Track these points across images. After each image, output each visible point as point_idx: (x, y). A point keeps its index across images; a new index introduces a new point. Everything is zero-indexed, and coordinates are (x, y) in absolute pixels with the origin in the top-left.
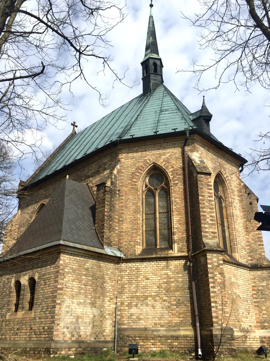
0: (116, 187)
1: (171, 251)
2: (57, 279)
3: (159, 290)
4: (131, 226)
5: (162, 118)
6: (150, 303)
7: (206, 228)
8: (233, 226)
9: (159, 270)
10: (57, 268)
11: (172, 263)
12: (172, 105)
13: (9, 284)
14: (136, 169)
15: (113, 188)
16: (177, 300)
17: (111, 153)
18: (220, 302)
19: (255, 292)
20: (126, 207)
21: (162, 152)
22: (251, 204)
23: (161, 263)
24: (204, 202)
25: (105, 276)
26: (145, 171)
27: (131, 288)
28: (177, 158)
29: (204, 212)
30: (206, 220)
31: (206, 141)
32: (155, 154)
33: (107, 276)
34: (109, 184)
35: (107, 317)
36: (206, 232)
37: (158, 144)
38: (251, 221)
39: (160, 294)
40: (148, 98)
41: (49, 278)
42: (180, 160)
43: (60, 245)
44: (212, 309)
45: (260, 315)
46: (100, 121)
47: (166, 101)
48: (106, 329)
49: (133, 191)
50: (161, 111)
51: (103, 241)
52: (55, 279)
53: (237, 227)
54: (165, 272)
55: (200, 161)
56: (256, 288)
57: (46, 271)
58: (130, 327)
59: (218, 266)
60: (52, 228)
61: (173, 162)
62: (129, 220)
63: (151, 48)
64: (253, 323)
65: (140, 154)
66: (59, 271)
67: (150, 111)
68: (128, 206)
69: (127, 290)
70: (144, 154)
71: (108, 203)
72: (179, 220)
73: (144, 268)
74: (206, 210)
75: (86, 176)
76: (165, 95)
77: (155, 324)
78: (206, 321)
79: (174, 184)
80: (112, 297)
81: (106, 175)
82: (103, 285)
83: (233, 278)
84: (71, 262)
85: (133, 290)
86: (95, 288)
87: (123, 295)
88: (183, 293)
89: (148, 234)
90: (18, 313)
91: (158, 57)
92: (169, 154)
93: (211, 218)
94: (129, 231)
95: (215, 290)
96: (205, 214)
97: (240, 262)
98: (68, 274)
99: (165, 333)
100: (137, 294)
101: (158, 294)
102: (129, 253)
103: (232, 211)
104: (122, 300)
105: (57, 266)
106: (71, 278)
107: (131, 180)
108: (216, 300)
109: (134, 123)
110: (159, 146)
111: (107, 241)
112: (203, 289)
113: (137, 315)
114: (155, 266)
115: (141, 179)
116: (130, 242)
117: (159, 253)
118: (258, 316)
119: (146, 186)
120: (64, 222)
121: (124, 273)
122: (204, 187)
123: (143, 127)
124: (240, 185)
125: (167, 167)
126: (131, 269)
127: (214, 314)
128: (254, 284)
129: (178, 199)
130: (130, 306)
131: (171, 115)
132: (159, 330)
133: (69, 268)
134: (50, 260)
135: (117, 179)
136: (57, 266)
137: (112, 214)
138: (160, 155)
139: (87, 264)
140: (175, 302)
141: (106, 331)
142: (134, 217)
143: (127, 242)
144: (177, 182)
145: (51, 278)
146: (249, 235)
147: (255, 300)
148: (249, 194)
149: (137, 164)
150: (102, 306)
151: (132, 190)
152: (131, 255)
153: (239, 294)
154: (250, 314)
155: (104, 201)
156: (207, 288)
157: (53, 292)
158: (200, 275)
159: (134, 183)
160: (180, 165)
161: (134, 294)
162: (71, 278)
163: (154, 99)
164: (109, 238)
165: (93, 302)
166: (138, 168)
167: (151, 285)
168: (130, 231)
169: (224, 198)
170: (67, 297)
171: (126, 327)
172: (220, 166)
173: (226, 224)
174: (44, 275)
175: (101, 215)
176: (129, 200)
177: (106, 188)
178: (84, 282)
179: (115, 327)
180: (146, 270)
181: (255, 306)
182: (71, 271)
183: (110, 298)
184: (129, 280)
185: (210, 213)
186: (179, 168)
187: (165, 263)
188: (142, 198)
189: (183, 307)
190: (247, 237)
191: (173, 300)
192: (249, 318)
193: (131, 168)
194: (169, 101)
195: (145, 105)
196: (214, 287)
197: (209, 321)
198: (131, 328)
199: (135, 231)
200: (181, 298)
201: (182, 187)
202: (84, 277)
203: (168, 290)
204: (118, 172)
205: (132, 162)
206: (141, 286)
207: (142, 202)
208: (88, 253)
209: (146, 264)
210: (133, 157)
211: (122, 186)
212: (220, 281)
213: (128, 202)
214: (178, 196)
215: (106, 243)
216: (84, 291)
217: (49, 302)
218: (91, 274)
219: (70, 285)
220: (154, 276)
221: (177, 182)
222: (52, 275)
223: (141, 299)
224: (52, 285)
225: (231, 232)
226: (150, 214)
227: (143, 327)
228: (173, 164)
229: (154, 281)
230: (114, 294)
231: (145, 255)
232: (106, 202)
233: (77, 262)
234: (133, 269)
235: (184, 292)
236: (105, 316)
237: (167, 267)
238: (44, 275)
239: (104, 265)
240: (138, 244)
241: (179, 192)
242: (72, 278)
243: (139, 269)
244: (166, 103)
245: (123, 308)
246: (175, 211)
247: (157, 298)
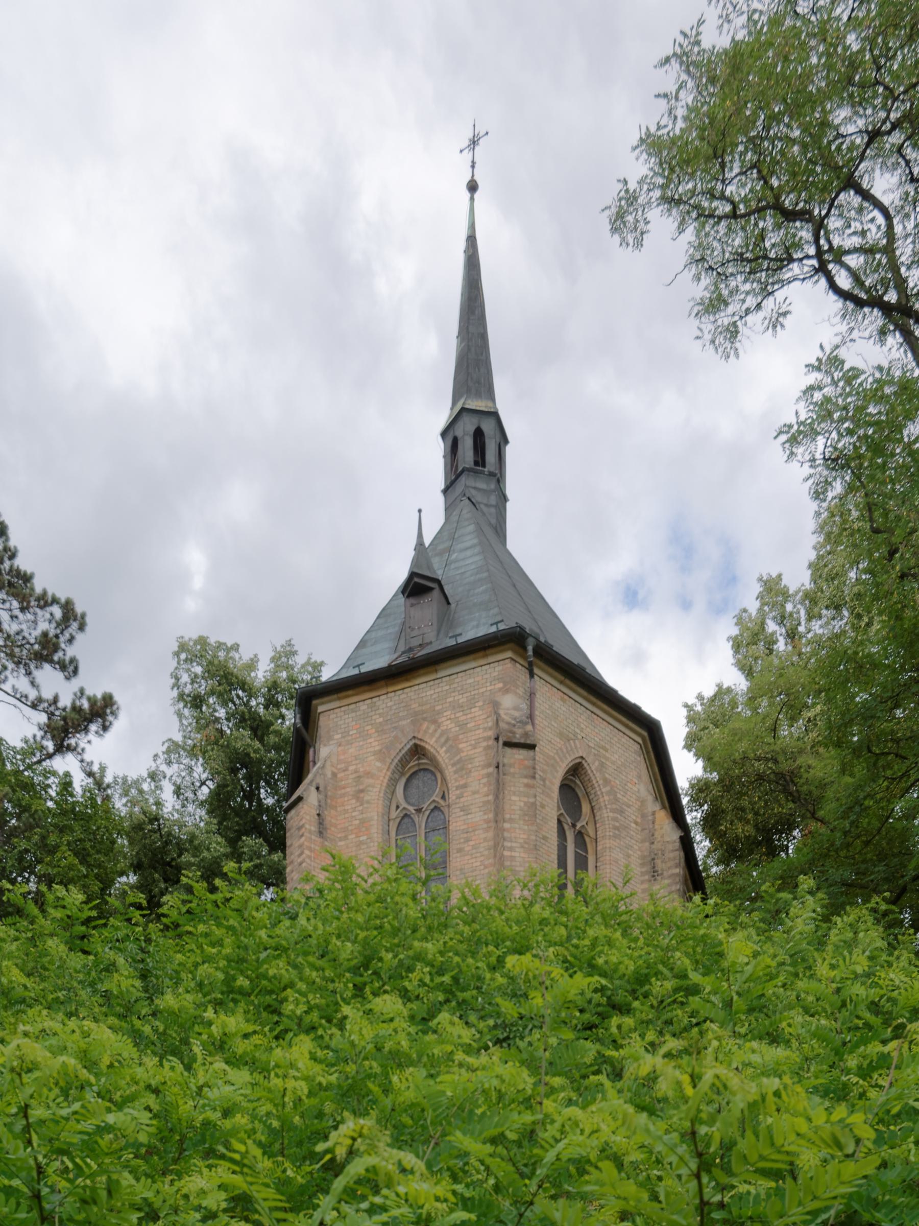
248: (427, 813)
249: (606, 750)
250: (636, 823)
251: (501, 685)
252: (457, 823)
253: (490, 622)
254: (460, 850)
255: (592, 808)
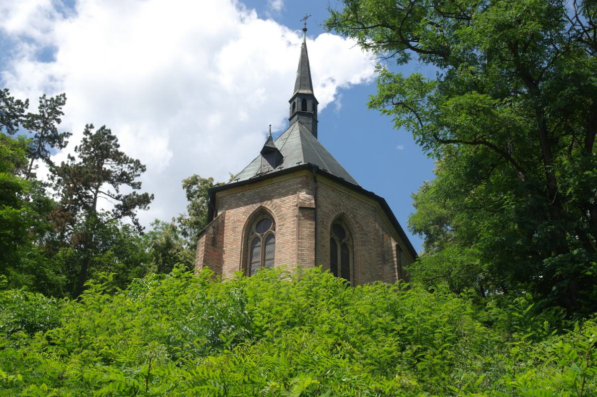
249: (357, 210)
250: (374, 239)
251: (301, 186)
252: (279, 240)
253: (297, 162)
254: (279, 251)
255: (351, 233)
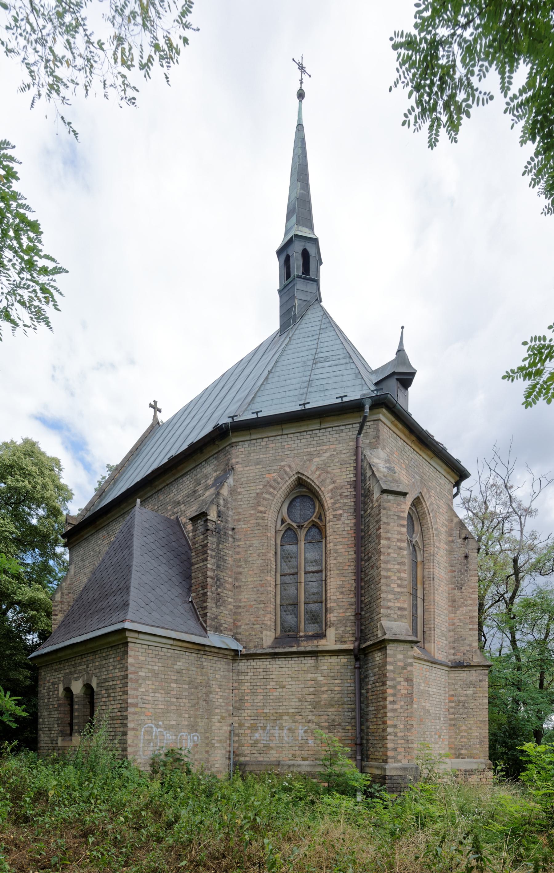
0: (227, 521)
1: (323, 642)
2: (125, 689)
3: (302, 705)
4: (255, 596)
5: (317, 377)
6: (287, 724)
7: (389, 600)
8: (432, 597)
9: (302, 672)
10: (124, 669)
11: (325, 661)
12: (337, 347)
13: (56, 692)
14: (265, 486)
15: (223, 524)
16: (330, 721)
17: (217, 453)
18: (402, 726)
19: (453, 704)
20: (246, 561)
21: (315, 449)
22: (466, 557)
23: (306, 662)
24: (390, 551)
25: (211, 682)
26: (282, 490)
27: (256, 701)
28: (343, 463)
29: (388, 570)
30: (389, 586)
31: (400, 426)
32: (302, 454)
33: (214, 682)
34: (213, 515)
35: (216, 745)
36: (389, 608)
37: (306, 431)
38: (463, 588)
39: (303, 710)
40: (290, 335)
41: (113, 687)
42: (348, 466)
43: (124, 630)
44: (388, 737)
45: (456, 738)
46: (200, 396)
47: (326, 339)
48: (215, 762)
49: (259, 531)
50: (316, 362)
51: (206, 623)
52: (122, 689)
53: (437, 598)
54: (313, 675)
55: (387, 467)
56: (455, 698)
57: (108, 674)
58: (254, 759)
59: (404, 668)
60: (114, 598)
61: (335, 471)
62: (252, 586)
63: (298, 214)
64: (445, 750)
65: (271, 455)
66: (127, 675)
67: (293, 361)
68: (250, 559)
69: (249, 704)
70: (280, 454)
71: (214, 553)
72: (341, 587)
73: (277, 669)
74: (392, 566)
75: (174, 502)
76: (323, 326)
77: (294, 756)
78: (377, 753)
79: (334, 516)
80: (224, 715)
81: (208, 499)
82: (207, 696)
83: (423, 685)
84: (148, 659)
85: (259, 704)
86: (195, 701)
87: (243, 711)
88: (340, 709)
89: (285, 611)
90: (73, 738)
91: (312, 236)
92: (328, 454)
93: (399, 582)
94: (251, 606)
95: (396, 707)
96: (389, 574)
97: (436, 658)
98: (144, 680)
99: (309, 769)
100: (265, 711)
101: (299, 710)
102: (252, 644)
103: (432, 570)
104: (241, 720)
105: (123, 667)
106: (150, 686)
107: (256, 509)
108: (395, 722)
109: (262, 389)
110: (309, 436)
111: (213, 623)
112: (375, 704)
113: (265, 742)
114: (296, 665)
115: (273, 506)
116: (254, 624)
117: (302, 644)
118: (454, 740)
119: (283, 522)
120: (132, 589)
121: (243, 678)
122: (392, 520)
123: (278, 396)
124: (452, 521)
125: (324, 481)
126: (255, 670)
127: (390, 745)
128: (453, 693)
129: (341, 547)
130: (253, 728)
131: (335, 368)
132: (299, 766)
133: (147, 670)
134: (113, 656)
135: (229, 506)
136: (123, 667)
137: (221, 573)
138: (311, 456)
139: (178, 663)
140: (327, 724)
141: (217, 766)
142: (261, 580)
143: (248, 624)
144: (340, 512)
145: (117, 686)
146: (455, 613)
147: (452, 716)
148: (465, 539)
149: (267, 476)
150: (208, 730)
151: (258, 528)
152: (255, 647)
153: (430, 708)
154: (442, 737)
155: (205, 549)
156: (382, 703)
157: (121, 710)
158: (371, 682)
159: (260, 515)
160: (348, 476)
161: (261, 711)
162: (150, 686)
163: (302, 335)
164: (216, 618)
165: (193, 724)
166: (268, 484)
167: (287, 697)
168: (255, 606)
169: (421, 547)
170: (146, 718)
171: (247, 759)
172: (421, 482)
173: (420, 594)
174: (106, 681)
175: (200, 575)
176: (251, 548)
177: (208, 524)
178: (175, 693)
179: (229, 759)
180: (281, 673)
181: (450, 725)
182: (150, 675)
183: (221, 716)
184: (251, 687)
185: (398, 572)
186: (346, 484)
187: (313, 661)
188: (274, 543)
189: (338, 732)
190: (453, 615)
191: (323, 721)
192: (440, 743)
193: (255, 484)
194: (331, 339)
195: (284, 350)
196: (394, 702)
197: (381, 754)
198: (255, 761)
199: (263, 605)
200: (336, 717)
201: (348, 522)
202: (175, 685)
203: (316, 705)
204: (233, 491)
205: (257, 470)
206: (271, 697)
207: (276, 553)
208: (180, 644)
209: (280, 663)
210: (258, 460)
211: (239, 520)
212: (405, 692)
213: (249, 552)
214: (341, 540)
215: (211, 626)
216: (175, 708)
217: (117, 726)
218: (187, 679)
219: (150, 698)
220: (294, 683)
221: (340, 512)
222: (118, 682)
223: (272, 718)
224: (118, 698)
225: (427, 607)
226: (289, 575)
227: (275, 759)
228: (334, 475)
229: (293, 690)
230: (227, 710)
231: (279, 647)
232: (209, 552)
233: (161, 661)
234: (258, 670)
235: (343, 708)
236: (213, 744)
237: (317, 667)
238: (106, 681)
239: (209, 664)
240: (265, 627)
241: (344, 533)
242: (154, 687)
243: (268, 670)
244: (326, 344)
245: (243, 731)
246: (335, 569)
247: (298, 717)
248: (307, 529)
